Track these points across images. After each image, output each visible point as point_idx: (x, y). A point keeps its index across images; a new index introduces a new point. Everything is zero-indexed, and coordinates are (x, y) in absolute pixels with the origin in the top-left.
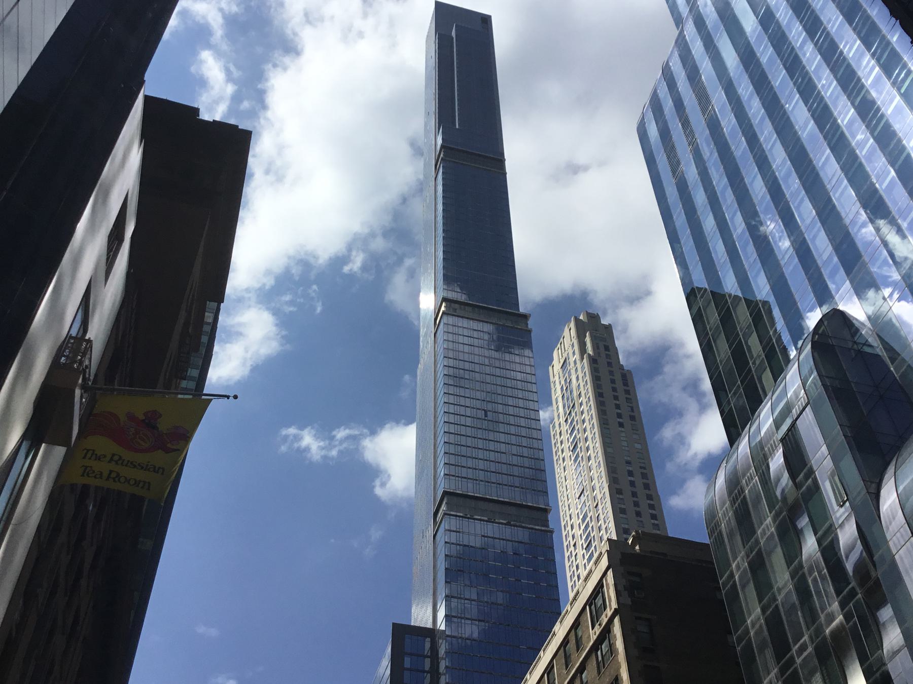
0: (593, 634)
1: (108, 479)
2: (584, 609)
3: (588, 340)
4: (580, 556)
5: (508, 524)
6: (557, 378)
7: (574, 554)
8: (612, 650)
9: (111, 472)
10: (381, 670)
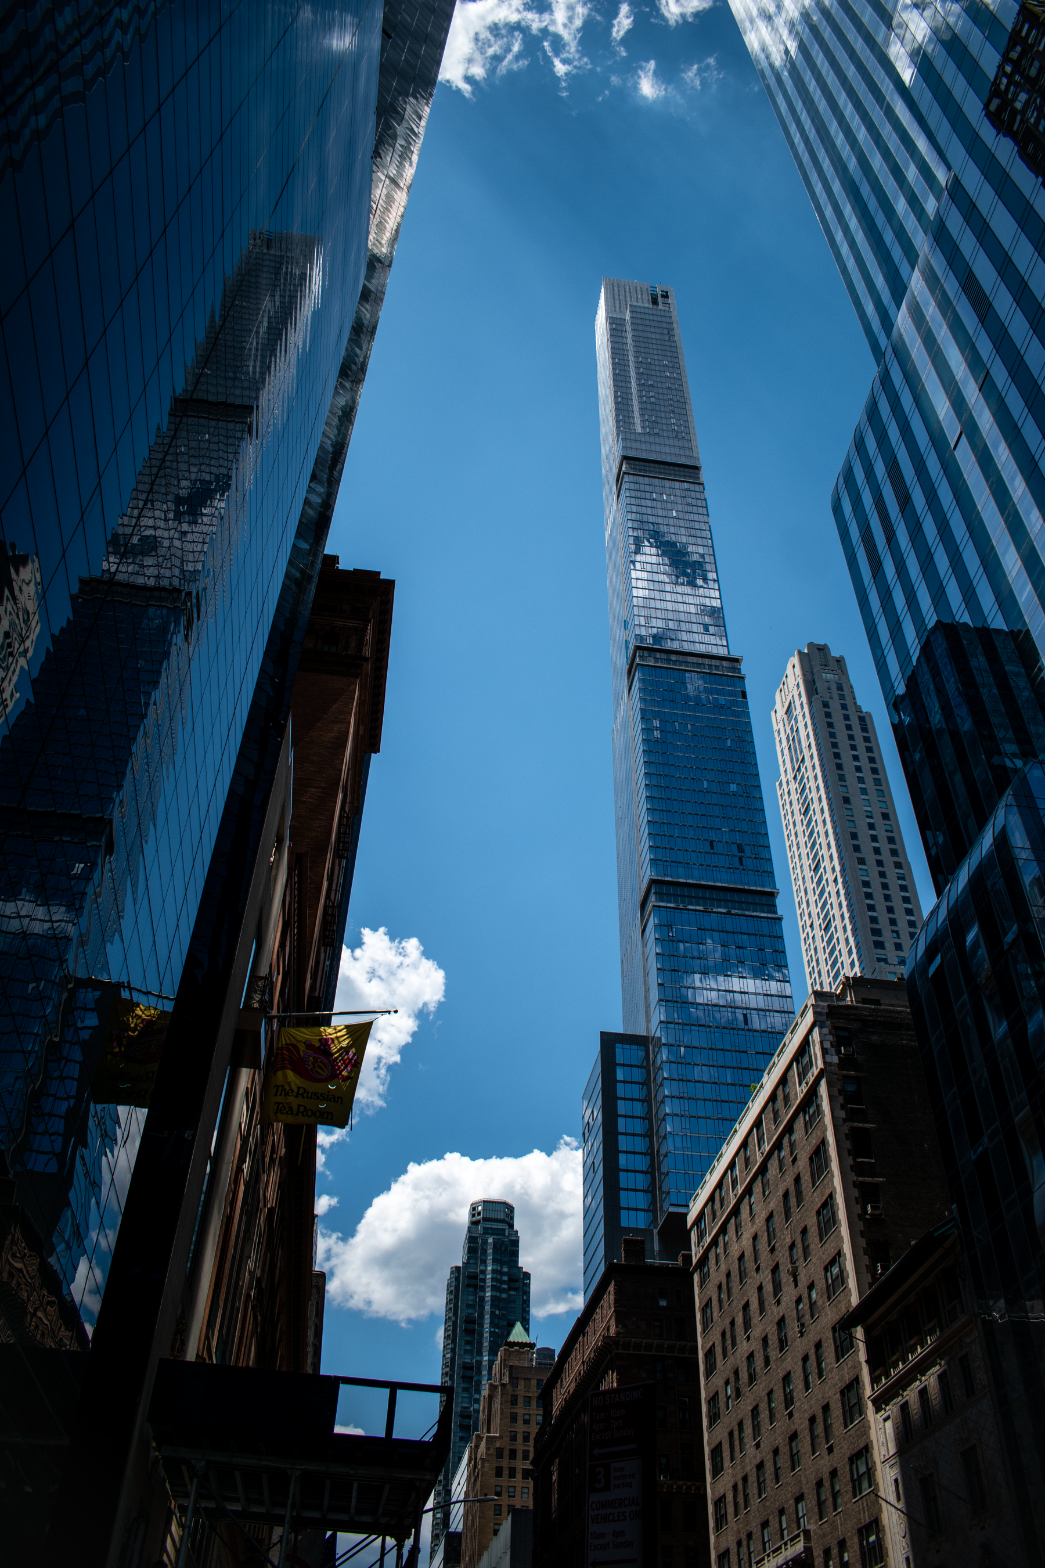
0: (799, 1091)
1: (297, 1114)
4: (818, 939)
5: (729, 913)
6: (781, 725)
7: (811, 936)
8: (819, 1111)
9: (299, 1106)
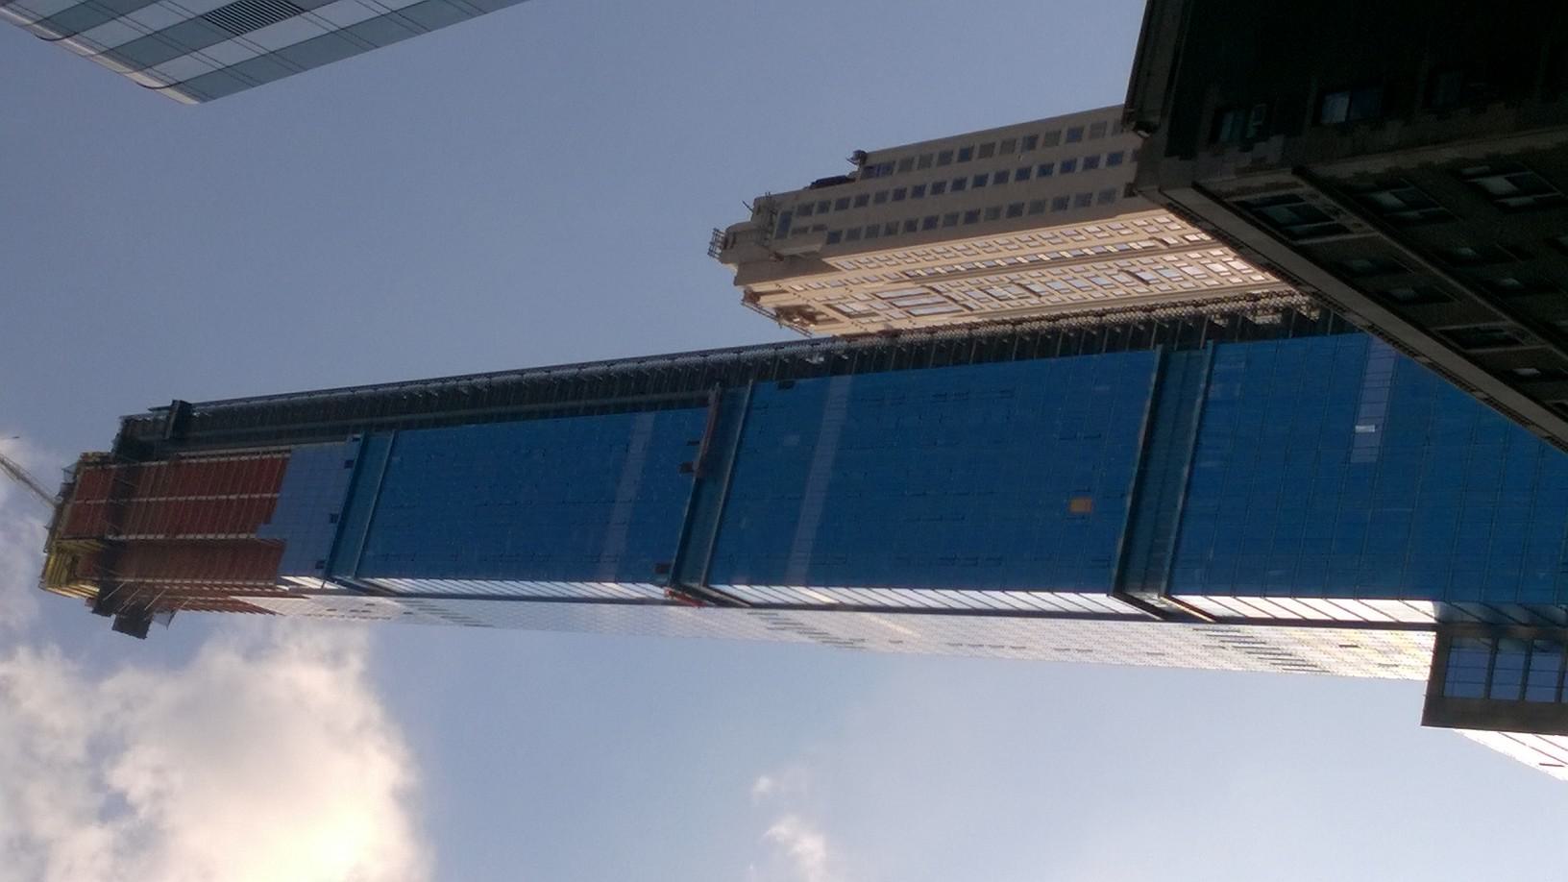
0: (1360, 231)
2: (1305, 253)
3: (742, 590)
8: (1390, 181)
10: (1532, 759)
